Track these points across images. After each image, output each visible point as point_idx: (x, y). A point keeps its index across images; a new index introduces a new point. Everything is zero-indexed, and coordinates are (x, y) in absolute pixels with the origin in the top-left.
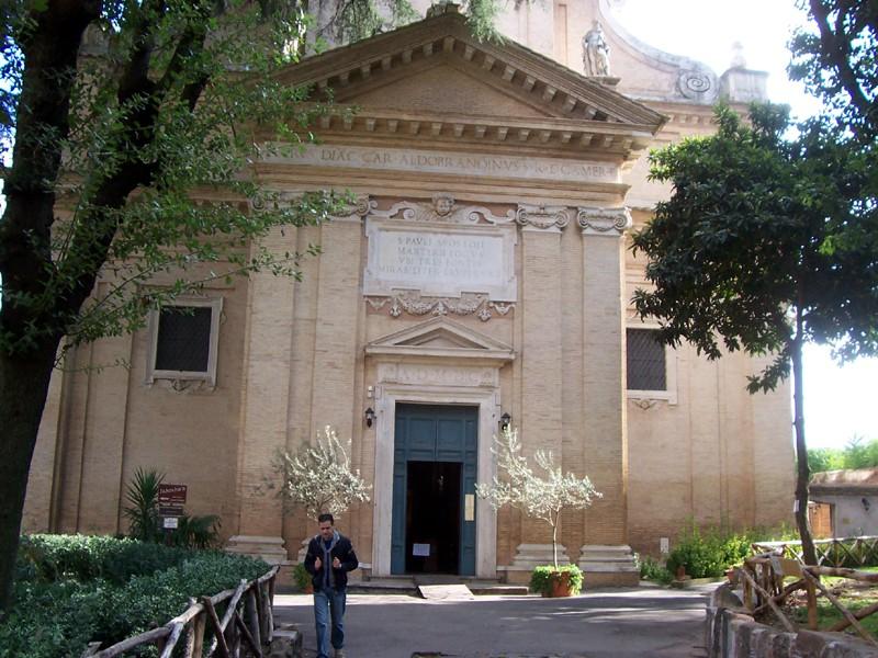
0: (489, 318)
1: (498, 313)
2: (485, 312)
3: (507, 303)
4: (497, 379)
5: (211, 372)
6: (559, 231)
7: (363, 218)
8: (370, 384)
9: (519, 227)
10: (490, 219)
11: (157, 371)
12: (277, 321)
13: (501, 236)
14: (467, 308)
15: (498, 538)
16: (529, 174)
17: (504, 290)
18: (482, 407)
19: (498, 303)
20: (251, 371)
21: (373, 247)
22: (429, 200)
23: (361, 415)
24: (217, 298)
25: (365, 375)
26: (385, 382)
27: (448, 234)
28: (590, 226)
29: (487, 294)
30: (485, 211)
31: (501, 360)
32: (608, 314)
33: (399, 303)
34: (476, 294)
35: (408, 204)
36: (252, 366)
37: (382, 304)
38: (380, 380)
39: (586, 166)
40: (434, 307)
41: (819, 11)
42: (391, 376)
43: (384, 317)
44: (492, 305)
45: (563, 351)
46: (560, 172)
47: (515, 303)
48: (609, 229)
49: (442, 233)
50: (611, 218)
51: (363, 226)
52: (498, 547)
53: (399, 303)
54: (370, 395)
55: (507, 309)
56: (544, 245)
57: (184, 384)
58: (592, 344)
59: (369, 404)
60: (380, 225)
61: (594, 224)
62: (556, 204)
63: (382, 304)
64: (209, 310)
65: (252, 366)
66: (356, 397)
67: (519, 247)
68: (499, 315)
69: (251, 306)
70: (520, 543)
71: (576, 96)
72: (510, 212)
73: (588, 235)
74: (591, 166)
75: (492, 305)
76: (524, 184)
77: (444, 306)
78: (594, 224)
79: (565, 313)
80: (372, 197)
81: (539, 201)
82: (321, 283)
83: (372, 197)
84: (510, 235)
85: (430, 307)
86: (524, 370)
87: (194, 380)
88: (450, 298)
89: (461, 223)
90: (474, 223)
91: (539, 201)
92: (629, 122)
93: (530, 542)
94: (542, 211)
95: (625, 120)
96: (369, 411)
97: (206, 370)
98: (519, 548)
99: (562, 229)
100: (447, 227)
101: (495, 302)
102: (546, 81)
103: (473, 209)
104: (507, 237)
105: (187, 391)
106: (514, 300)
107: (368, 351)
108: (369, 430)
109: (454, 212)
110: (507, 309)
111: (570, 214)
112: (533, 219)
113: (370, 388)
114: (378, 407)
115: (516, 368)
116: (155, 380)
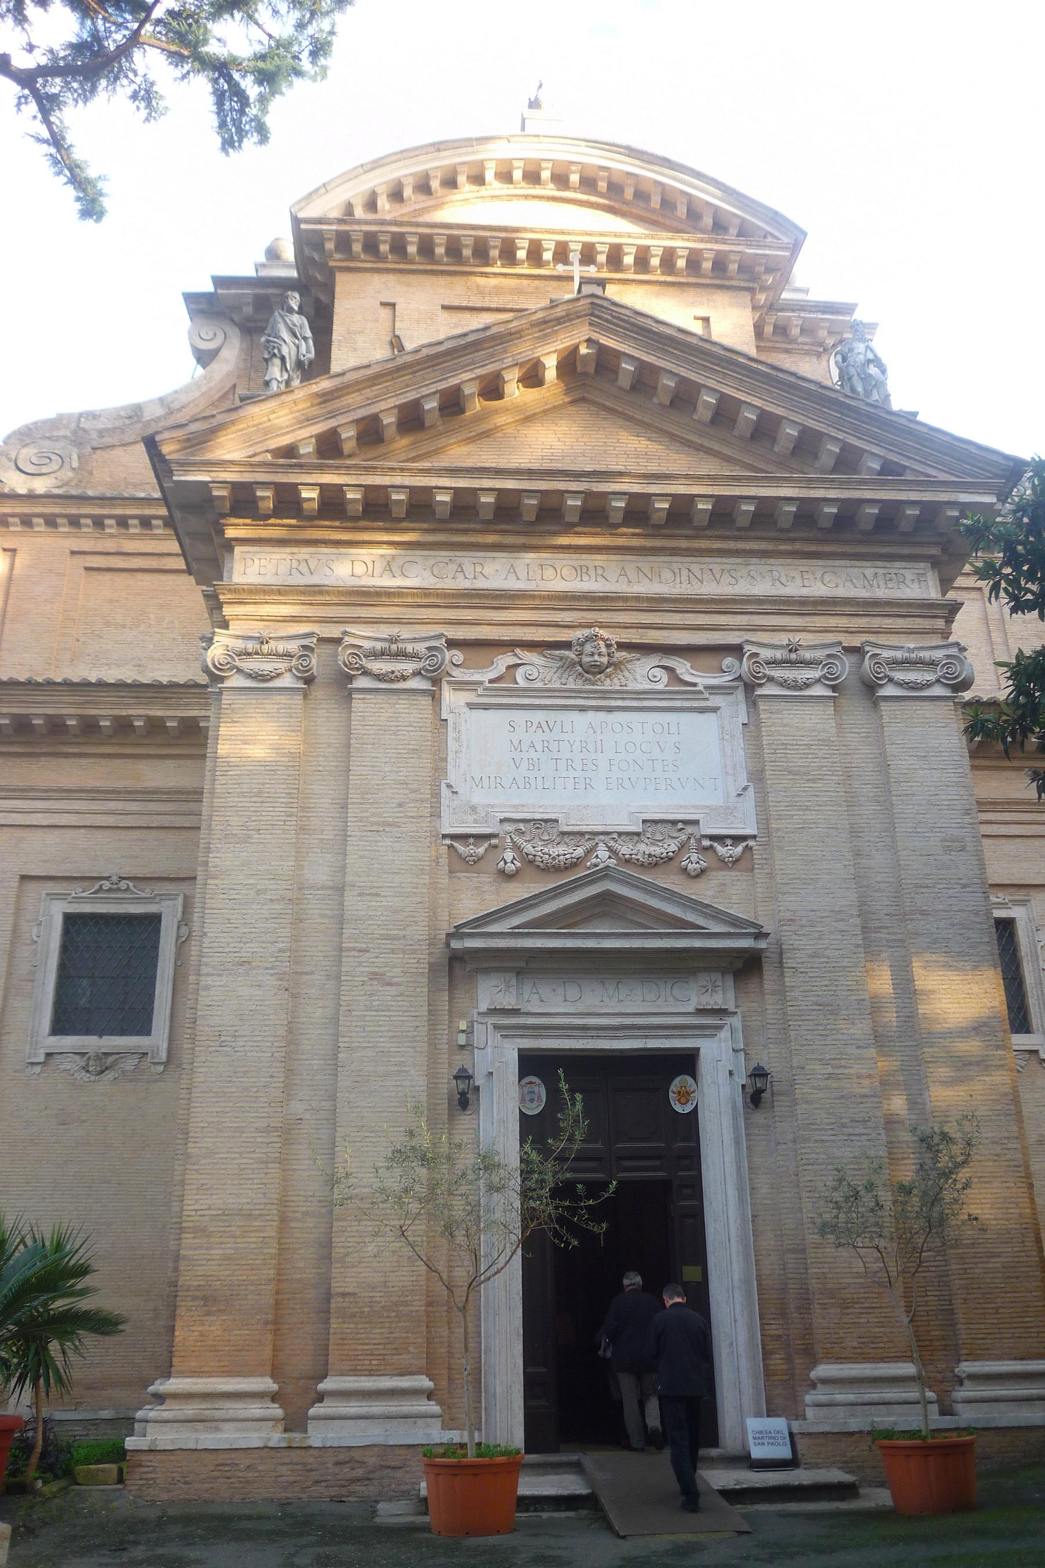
0: (703, 871)
1: (722, 860)
2: (694, 857)
3: (737, 839)
4: (731, 994)
5: (158, 1039)
6: (829, 693)
7: (436, 682)
8: (462, 1016)
9: (750, 688)
10: (687, 678)
11: (53, 1039)
12: (258, 892)
13: (715, 710)
14: (656, 850)
15: (766, 1354)
16: (762, 588)
17: (729, 811)
18: (703, 1052)
19: (720, 839)
20: (204, 998)
21: (457, 739)
22: (567, 645)
23: (446, 1085)
24: (173, 897)
25: (451, 1000)
26: (493, 1011)
27: (610, 710)
28: (891, 680)
29: (696, 822)
30: (683, 667)
31: (775, 1335)
32: (948, 850)
33: (517, 848)
34: (674, 823)
35: (527, 656)
36: (207, 988)
37: (481, 850)
38: (483, 1007)
39: (869, 572)
40: (589, 852)
41: (923, 1257)
42: (508, 1001)
43: (485, 878)
44: (706, 843)
45: (865, 929)
46: (819, 584)
47: (754, 837)
48: (928, 685)
49: (597, 709)
50: (932, 664)
51: (435, 697)
52: (768, 1373)
53: (517, 848)
54: (462, 1039)
55: (740, 849)
56: (804, 723)
57: (102, 1064)
58: (924, 913)
59: (461, 1060)
60: (470, 697)
61: (899, 676)
62: (812, 637)
63: (481, 850)
64: (153, 921)
65: (207, 988)
66: (433, 1044)
67: (752, 728)
68: (725, 864)
69: (206, 864)
70: (814, 1363)
71: (840, 436)
72: (728, 661)
73: (887, 698)
74: (881, 571)
75: (706, 843)
76: (751, 608)
77: (610, 849)
78: (899, 676)
79: (858, 854)
80: (452, 644)
81: (783, 639)
82: (352, 811)
83: (452, 644)
84: (734, 710)
85: (580, 852)
86: (788, 973)
87: (121, 1055)
88: (620, 834)
89: (632, 686)
90: (660, 686)
91: (783, 639)
92: (943, 477)
93: (839, 1359)
94: (793, 656)
95: (933, 472)
96: (464, 1076)
97: (148, 1033)
98: (813, 1374)
99: (834, 688)
100: (605, 694)
101: (712, 838)
102: (779, 411)
103: (654, 660)
104: (725, 711)
105: (110, 1075)
106: (754, 832)
107: (456, 944)
108: (465, 1120)
109: (617, 666)
110: (740, 849)
111: (848, 661)
112: (777, 673)
113: (463, 1025)
114: (481, 1064)
115: (769, 972)
116: (49, 1055)
